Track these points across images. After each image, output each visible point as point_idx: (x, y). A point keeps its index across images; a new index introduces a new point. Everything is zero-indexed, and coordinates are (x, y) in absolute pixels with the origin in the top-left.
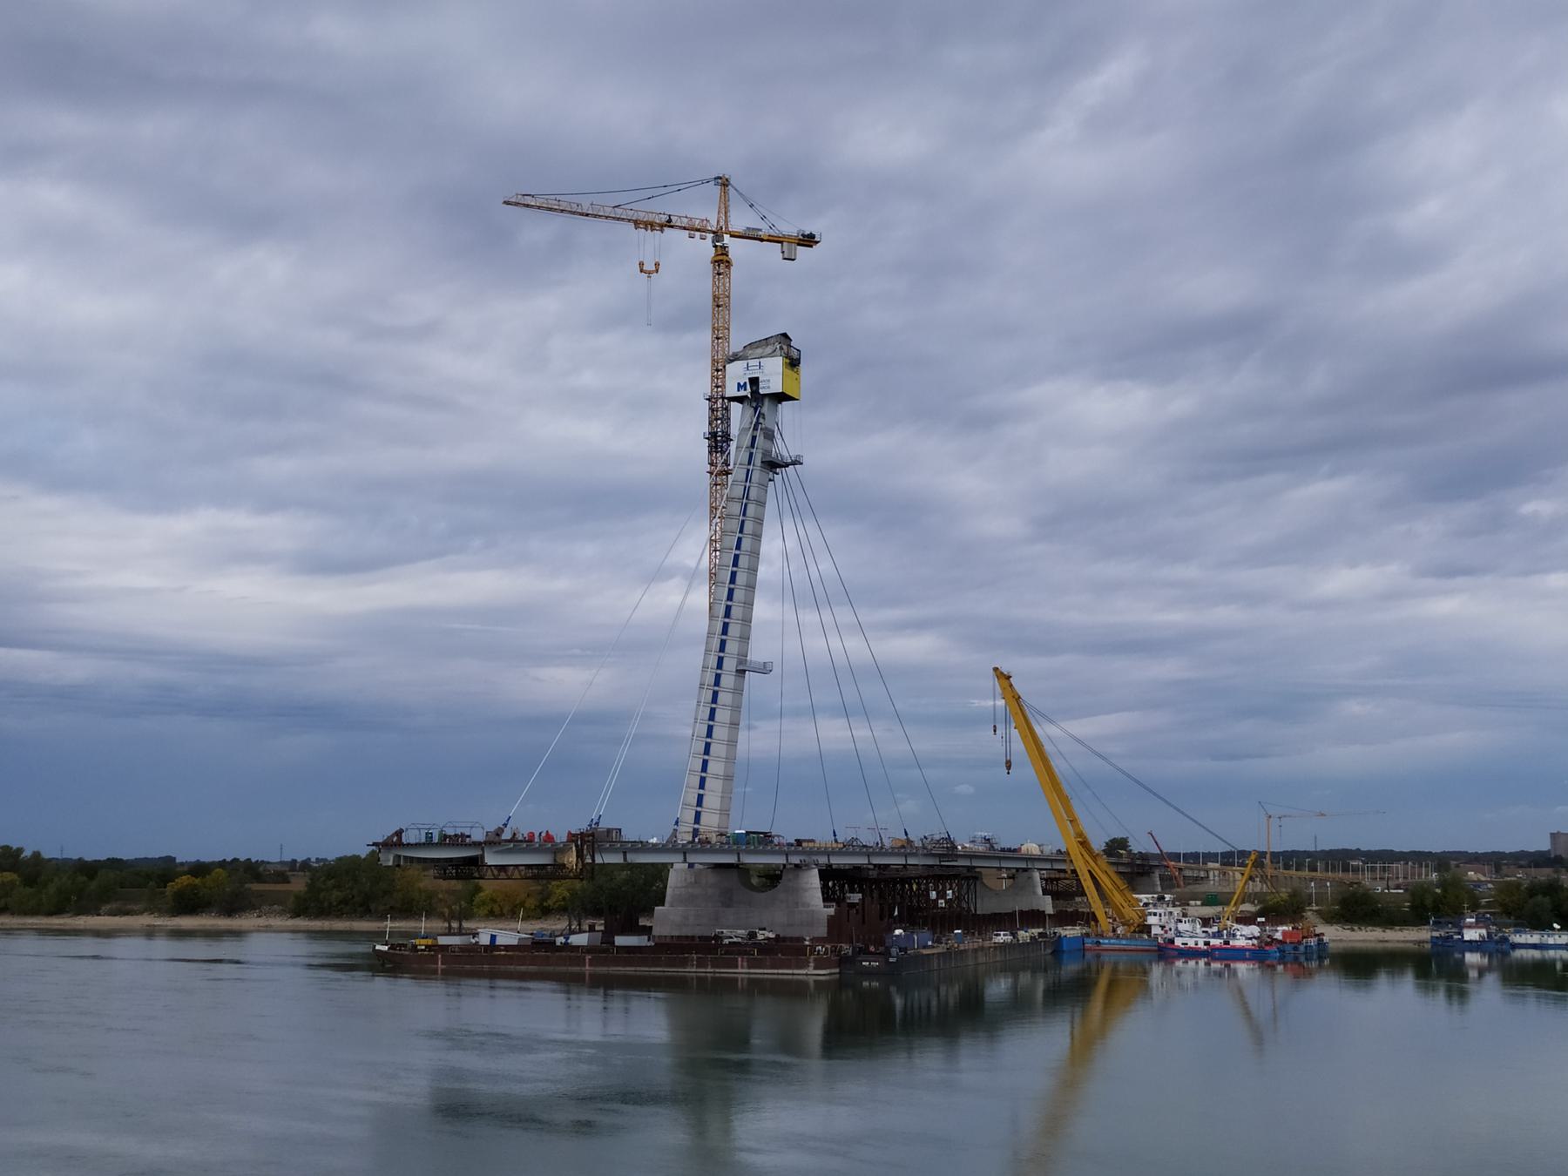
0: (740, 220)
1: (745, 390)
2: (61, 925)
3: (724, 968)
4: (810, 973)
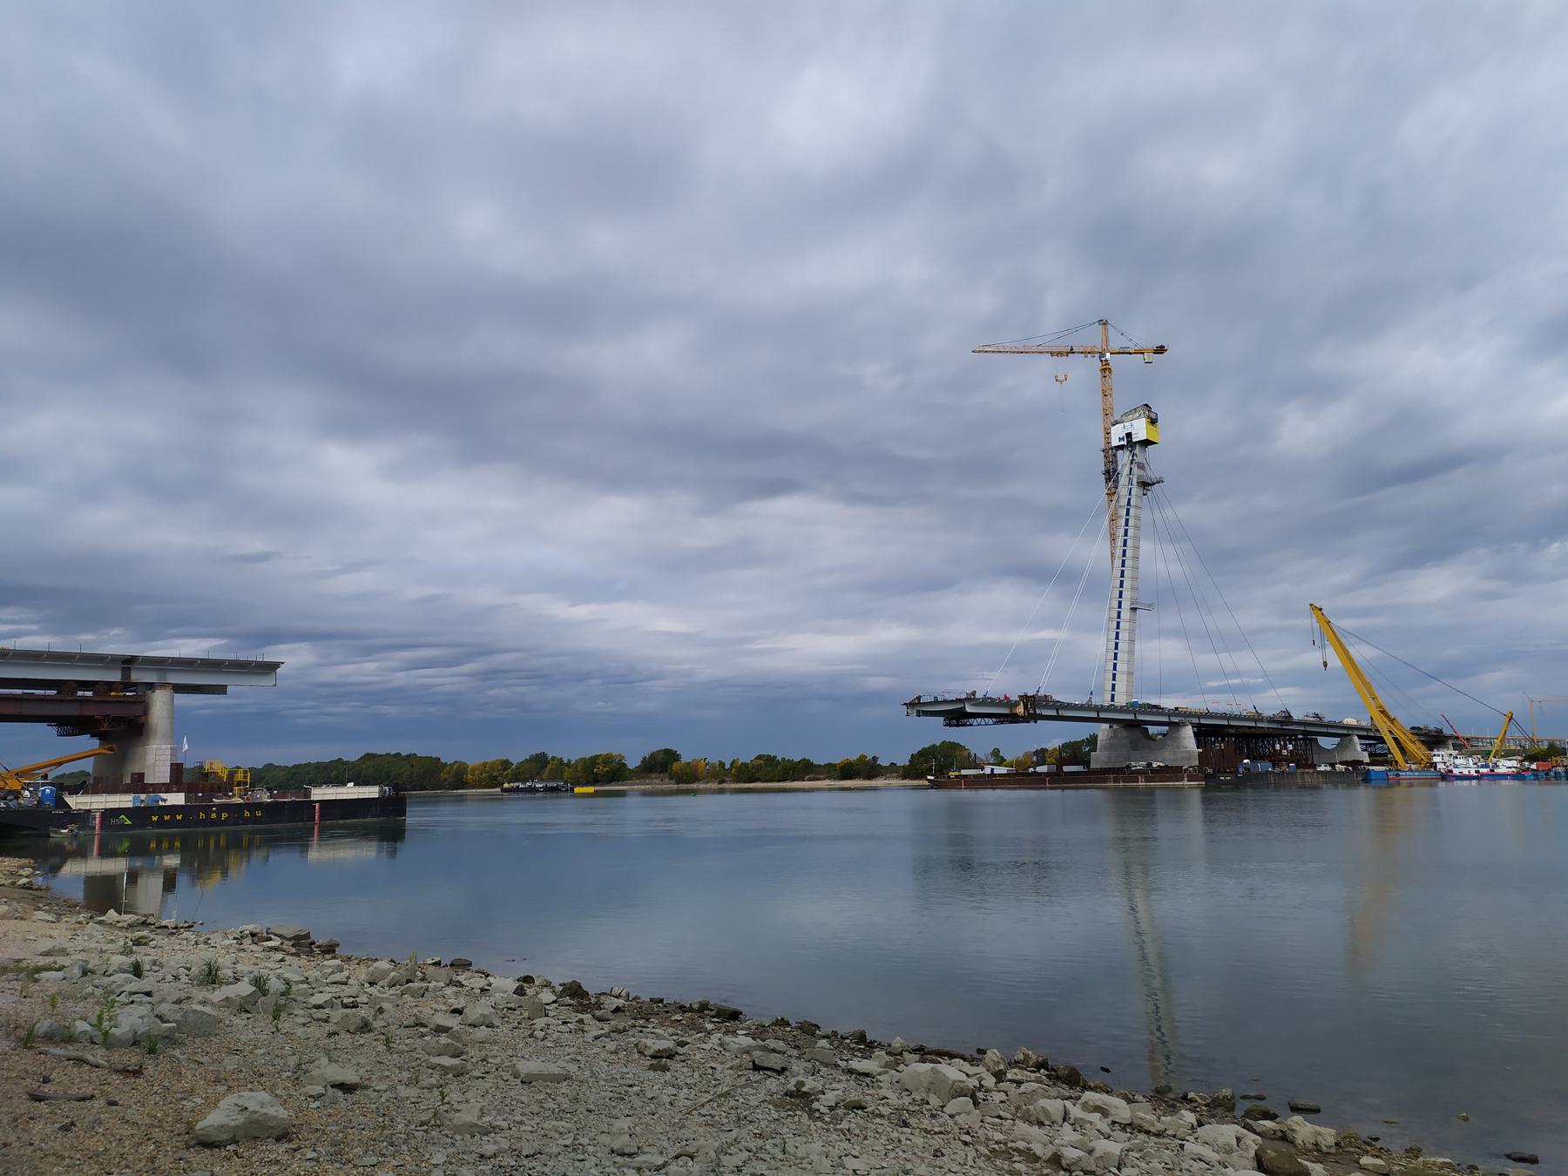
0: (1116, 343)
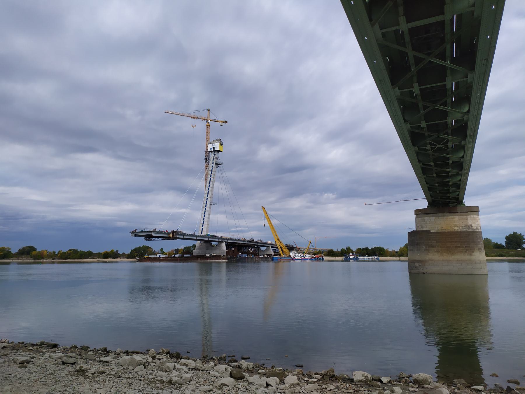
0: (212, 118)
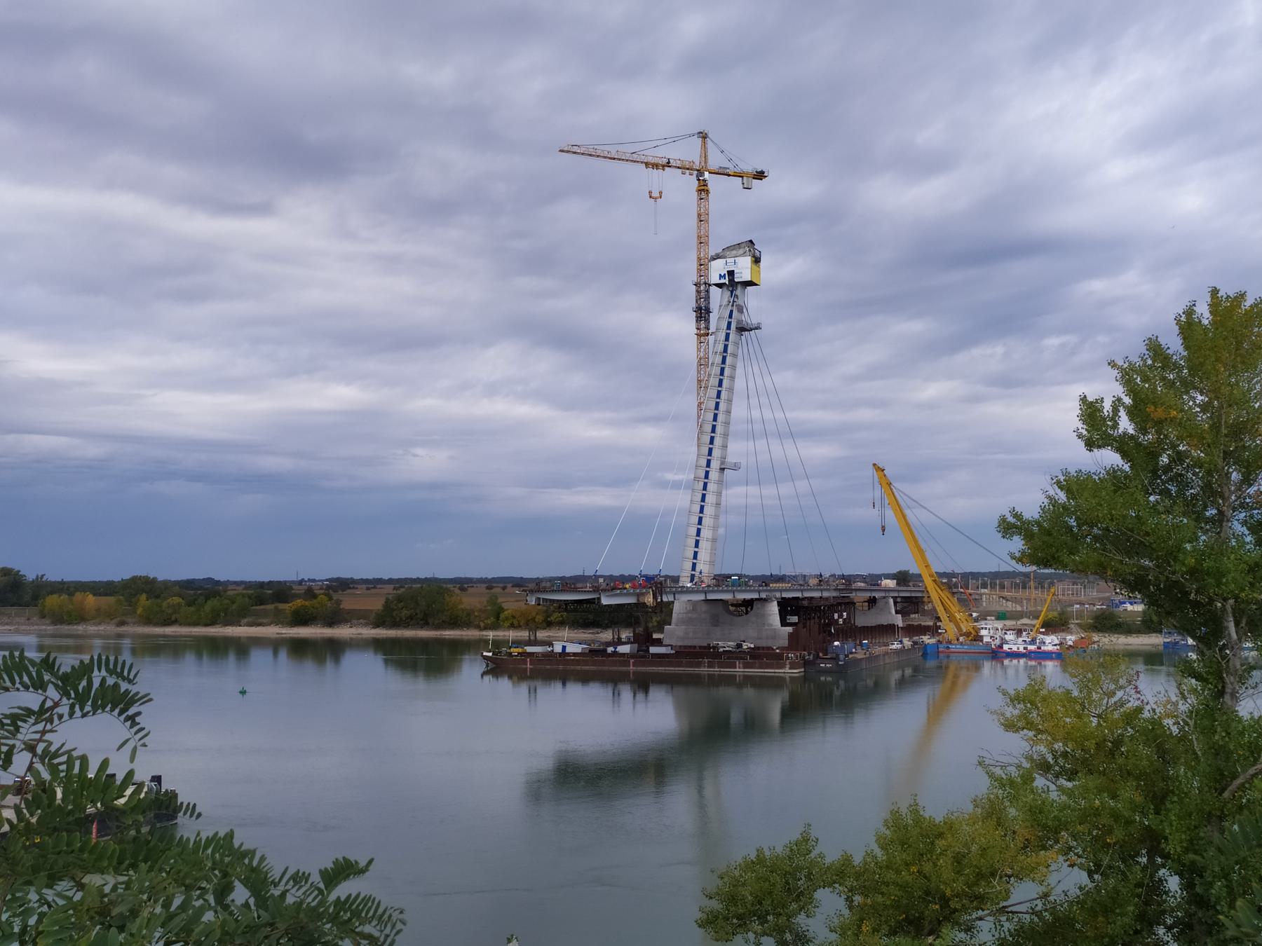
0: (715, 161)
1: (725, 279)
2: (215, 632)
3: (727, 668)
4: (787, 672)
